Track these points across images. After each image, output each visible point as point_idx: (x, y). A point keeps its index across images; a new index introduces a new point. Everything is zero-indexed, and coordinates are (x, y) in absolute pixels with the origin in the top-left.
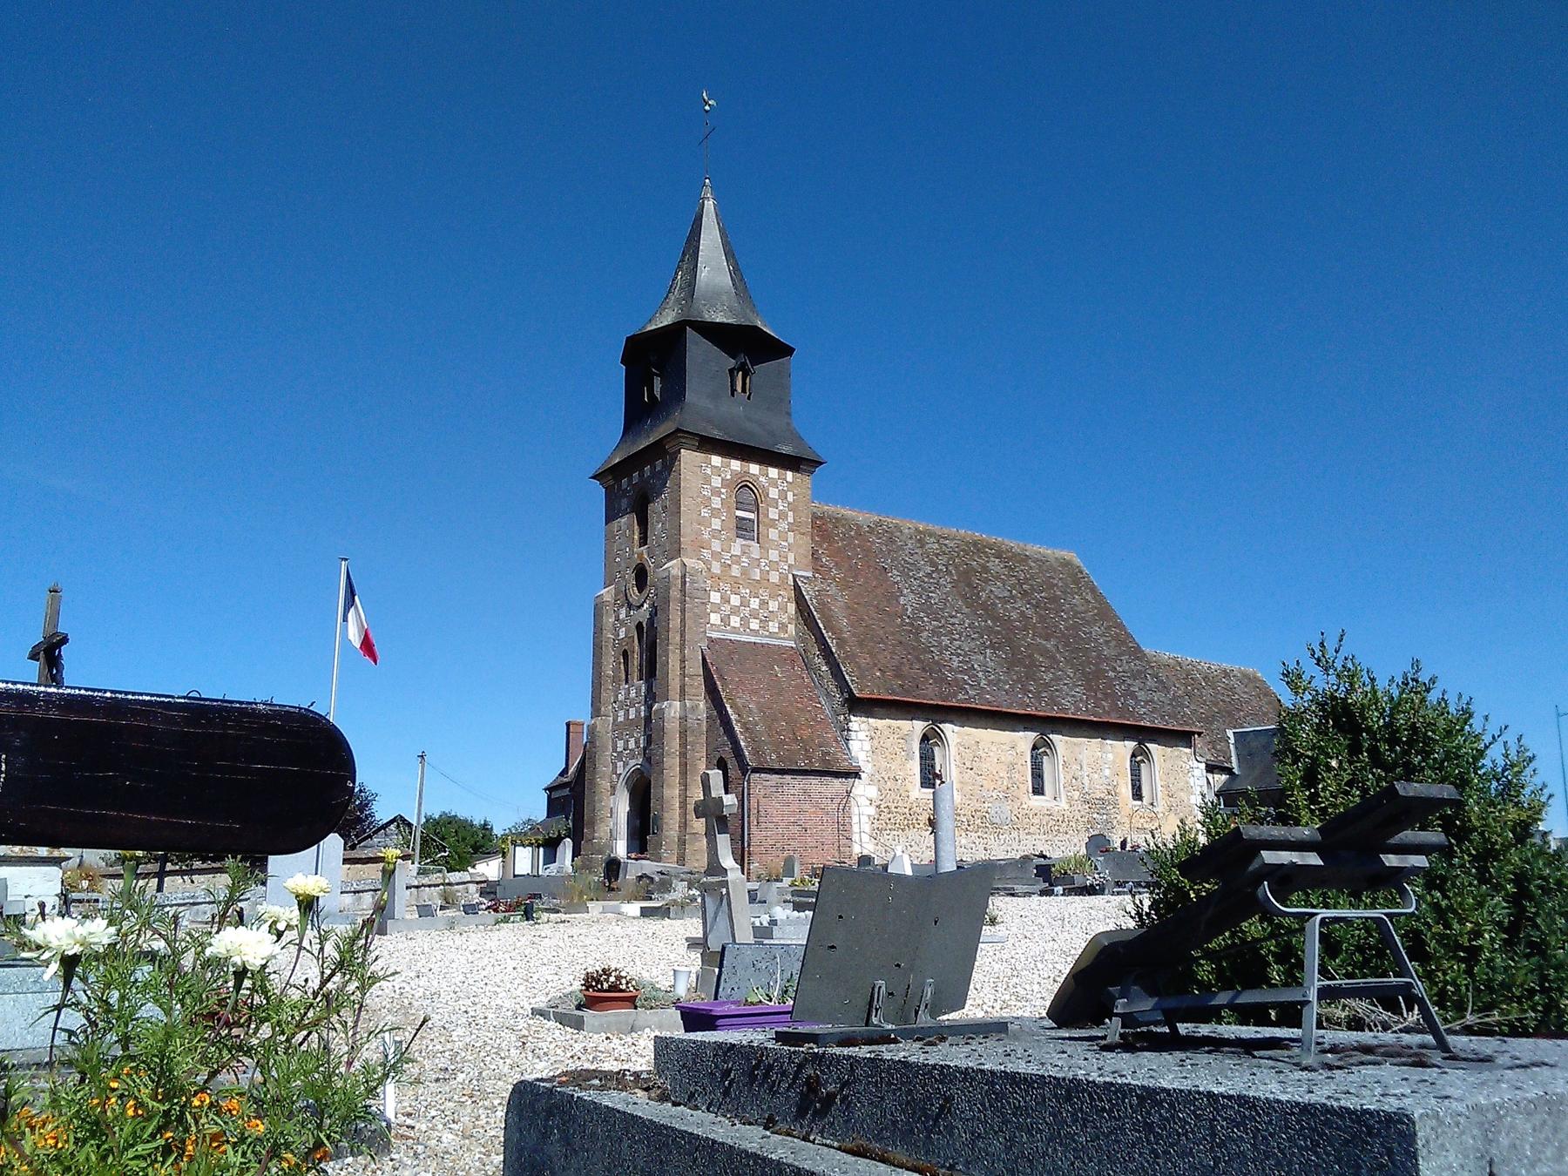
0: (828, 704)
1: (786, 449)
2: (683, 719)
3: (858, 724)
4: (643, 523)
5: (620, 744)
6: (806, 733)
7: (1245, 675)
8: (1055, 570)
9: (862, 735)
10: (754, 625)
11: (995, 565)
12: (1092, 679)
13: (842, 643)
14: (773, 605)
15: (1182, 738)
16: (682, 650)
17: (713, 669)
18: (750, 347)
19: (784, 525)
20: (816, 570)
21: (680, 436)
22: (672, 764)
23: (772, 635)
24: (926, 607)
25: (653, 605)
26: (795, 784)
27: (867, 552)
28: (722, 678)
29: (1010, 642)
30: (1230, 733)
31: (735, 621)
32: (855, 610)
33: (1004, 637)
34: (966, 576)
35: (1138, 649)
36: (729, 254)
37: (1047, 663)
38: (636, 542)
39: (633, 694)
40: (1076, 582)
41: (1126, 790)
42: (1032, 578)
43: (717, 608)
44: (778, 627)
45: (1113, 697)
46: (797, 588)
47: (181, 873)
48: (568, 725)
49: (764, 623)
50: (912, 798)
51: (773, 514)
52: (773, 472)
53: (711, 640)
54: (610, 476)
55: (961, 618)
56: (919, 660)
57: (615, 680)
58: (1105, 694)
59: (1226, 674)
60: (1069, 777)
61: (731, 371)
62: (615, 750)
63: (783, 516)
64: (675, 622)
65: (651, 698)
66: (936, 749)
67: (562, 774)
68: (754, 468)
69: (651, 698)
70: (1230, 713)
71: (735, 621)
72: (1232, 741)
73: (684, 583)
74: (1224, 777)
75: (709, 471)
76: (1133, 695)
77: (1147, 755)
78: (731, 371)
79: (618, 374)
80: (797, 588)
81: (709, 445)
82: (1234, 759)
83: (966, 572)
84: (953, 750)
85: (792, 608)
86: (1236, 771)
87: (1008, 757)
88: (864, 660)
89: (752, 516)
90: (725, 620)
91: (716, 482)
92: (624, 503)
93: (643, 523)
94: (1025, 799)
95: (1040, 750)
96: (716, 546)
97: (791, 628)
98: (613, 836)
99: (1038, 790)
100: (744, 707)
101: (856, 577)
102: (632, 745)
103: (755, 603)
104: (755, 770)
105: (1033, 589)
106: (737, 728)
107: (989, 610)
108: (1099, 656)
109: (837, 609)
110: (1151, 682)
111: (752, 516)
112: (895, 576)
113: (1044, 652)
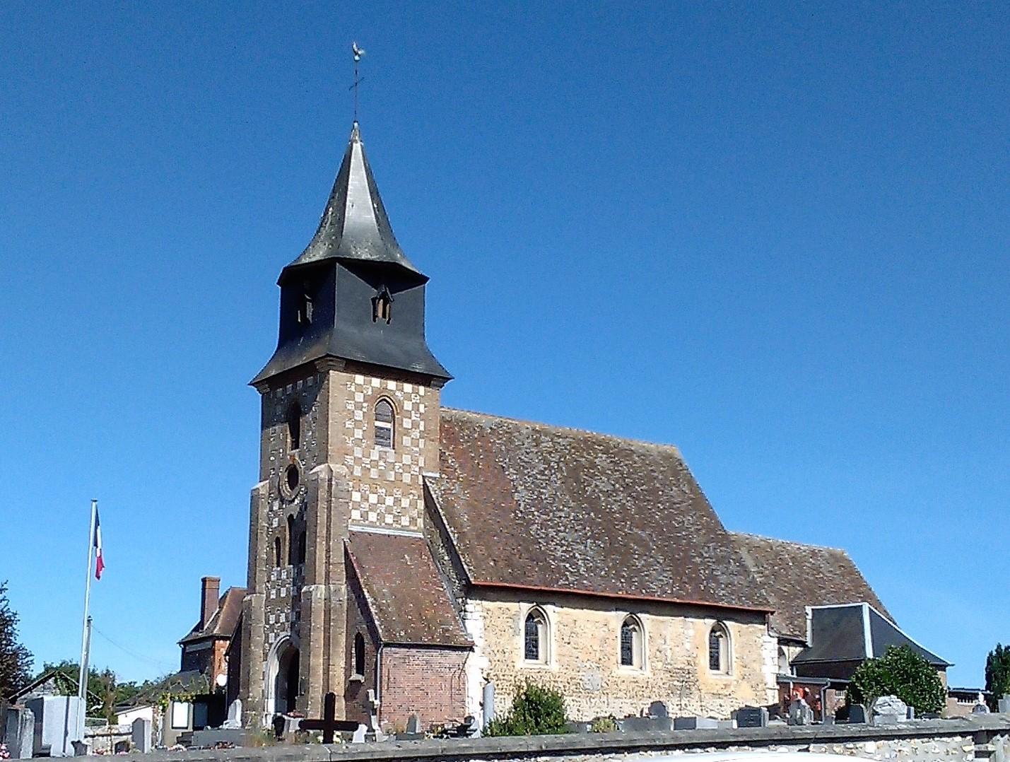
0: (448, 590)
1: (419, 368)
2: (327, 600)
3: (473, 606)
5: (272, 619)
6: (430, 614)
7: (832, 555)
8: (657, 464)
9: (476, 615)
11: (602, 460)
12: (679, 566)
13: (462, 536)
14: (405, 503)
15: (760, 616)
16: (328, 543)
17: (353, 559)
18: (391, 278)
19: (416, 434)
20: (442, 471)
21: (332, 361)
22: (318, 637)
23: (403, 528)
24: (538, 502)
25: (302, 501)
26: (423, 655)
27: (488, 451)
28: (361, 567)
30: (809, 609)
31: (373, 517)
32: (474, 507)
33: (605, 529)
34: (574, 472)
35: (726, 536)
36: (374, 193)
37: (641, 550)
38: (289, 445)
39: (284, 576)
40: (676, 474)
41: (704, 660)
42: (635, 472)
43: (357, 506)
45: (695, 581)
46: (425, 487)
48: (204, 580)
49: (397, 519)
51: (407, 423)
52: (408, 387)
53: (353, 534)
54: (268, 385)
55: (567, 512)
56: (528, 550)
57: (268, 561)
58: (691, 579)
59: (814, 554)
60: (654, 650)
61: (374, 300)
62: (267, 622)
63: (415, 425)
64: (322, 517)
65: (299, 580)
66: (539, 626)
67: (196, 629)
68: (392, 385)
69: (299, 580)
70: (812, 592)
71: (373, 517)
72: (810, 617)
73: (330, 486)
74: (799, 649)
75: (353, 389)
76: (715, 579)
77: (724, 630)
78: (374, 300)
79: (275, 294)
80: (425, 487)
81: (354, 366)
83: (575, 469)
84: (554, 628)
86: (809, 644)
87: (601, 633)
88: (480, 551)
89: (389, 426)
90: (364, 516)
91: (359, 397)
92: (279, 410)
94: (614, 668)
95: (628, 628)
96: (358, 453)
97: (420, 521)
98: (265, 696)
99: (627, 660)
100: (378, 592)
102: (283, 619)
103: (389, 501)
104: (387, 645)
105: (634, 483)
106: (373, 610)
107: (593, 504)
108: (688, 544)
111: (389, 426)
112: (511, 474)
113: (640, 542)
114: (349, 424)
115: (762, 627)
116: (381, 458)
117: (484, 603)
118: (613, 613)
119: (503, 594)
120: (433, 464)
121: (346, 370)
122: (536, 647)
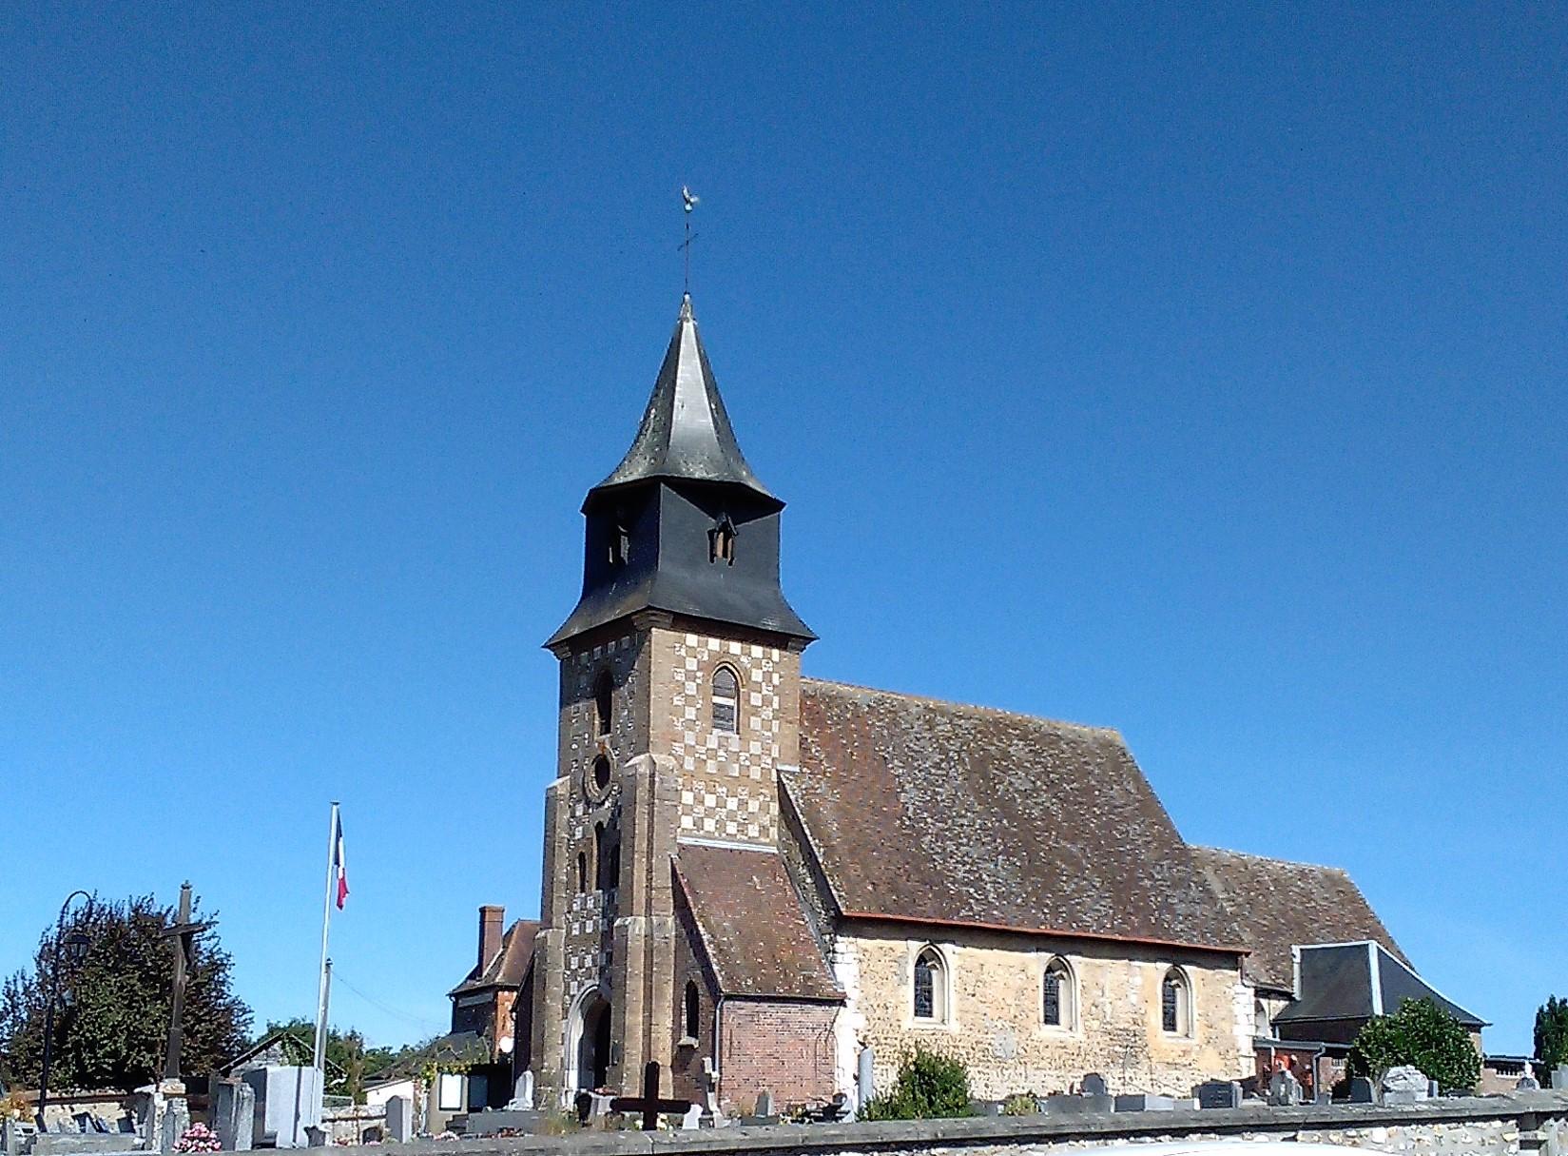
0: (811, 923)
1: (772, 625)
2: (649, 937)
3: (845, 945)
4: (606, 712)
5: (574, 963)
6: (786, 955)
8: (1092, 753)
10: (732, 828)
11: (1018, 749)
12: (1122, 890)
13: (830, 850)
14: (753, 806)
15: (1230, 959)
16: (649, 861)
17: (683, 881)
18: (734, 504)
20: (803, 764)
21: (653, 615)
22: (636, 987)
23: (751, 840)
24: (932, 806)
25: (615, 804)
26: (777, 1011)
28: (694, 892)
29: (1026, 846)
30: (1296, 950)
31: (710, 825)
32: (846, 812)
34: (981, 765)
35: (1185, 850)
36: (712, 389)
37: (1070, 870)
38: (597, 729)
39: (590, 905)
40: (1117, 767)
42: (1063, 765)
43: (689, 810)
44: (759, 831)
45: (1143, 911)
46: (781, 785)
47: (61, 1101)
48: (483, 911)
49: (742, 827)
50: (905, 1027)
51: (756, 699)
52: (757, 651)
53: (683, 848)
54: (568, 647)
55: (971, 819)
56: (917, 869)
57: (568, 885)
59: (1303, 874)
61: (711, 533)
62: (568, 966)
63: (767, 701)
64: (641, 826)
65: (611, 910)
67: (471, 977)
68: (735, 647)
69: (611, 910)
70: (1301, 926)
71: (710, 825)
72: (1297, 960)
73: (652, 783)
74: (1282, 1004)
75: (683, 652)
76: (1170, 908)
77: (1183, 978)
78: (711, 533)
80: (781, 785)
81: (684, 622)
82: (1296, 982)
83: (982, 761)
84: (953, 974)
85: (775, 808)
86: (1297, 996)
87: (1017, 981)
88: (855, 871)
89: (731, 702)
90: (698, 824)
91: (692, 664)
93: (606, 712)
94: (1034, 1029)
96: (690, 739)
97: (774, 831)
98: (564, 1066)
99: (1051, 1018)
100: (717, 926)
101: (850, 772)
103: (732, 804)
104: (729, 998)
105: (1062, 779)
106: (710, 950)
107: (1007, 808)
108: (1134, 861)
109: (825, 812)
110: (1194, 893)
111: (731, 702)
112: (896, 767)
113: (1069, 858)
114: (678, 701)
115: (1233, 973)
116: (720, 746)
117: (860, 941)
118: (1033, 955)
119: (885, 928)
120: (791, 754)
121: (673, 627)
122: (930, 1000)
